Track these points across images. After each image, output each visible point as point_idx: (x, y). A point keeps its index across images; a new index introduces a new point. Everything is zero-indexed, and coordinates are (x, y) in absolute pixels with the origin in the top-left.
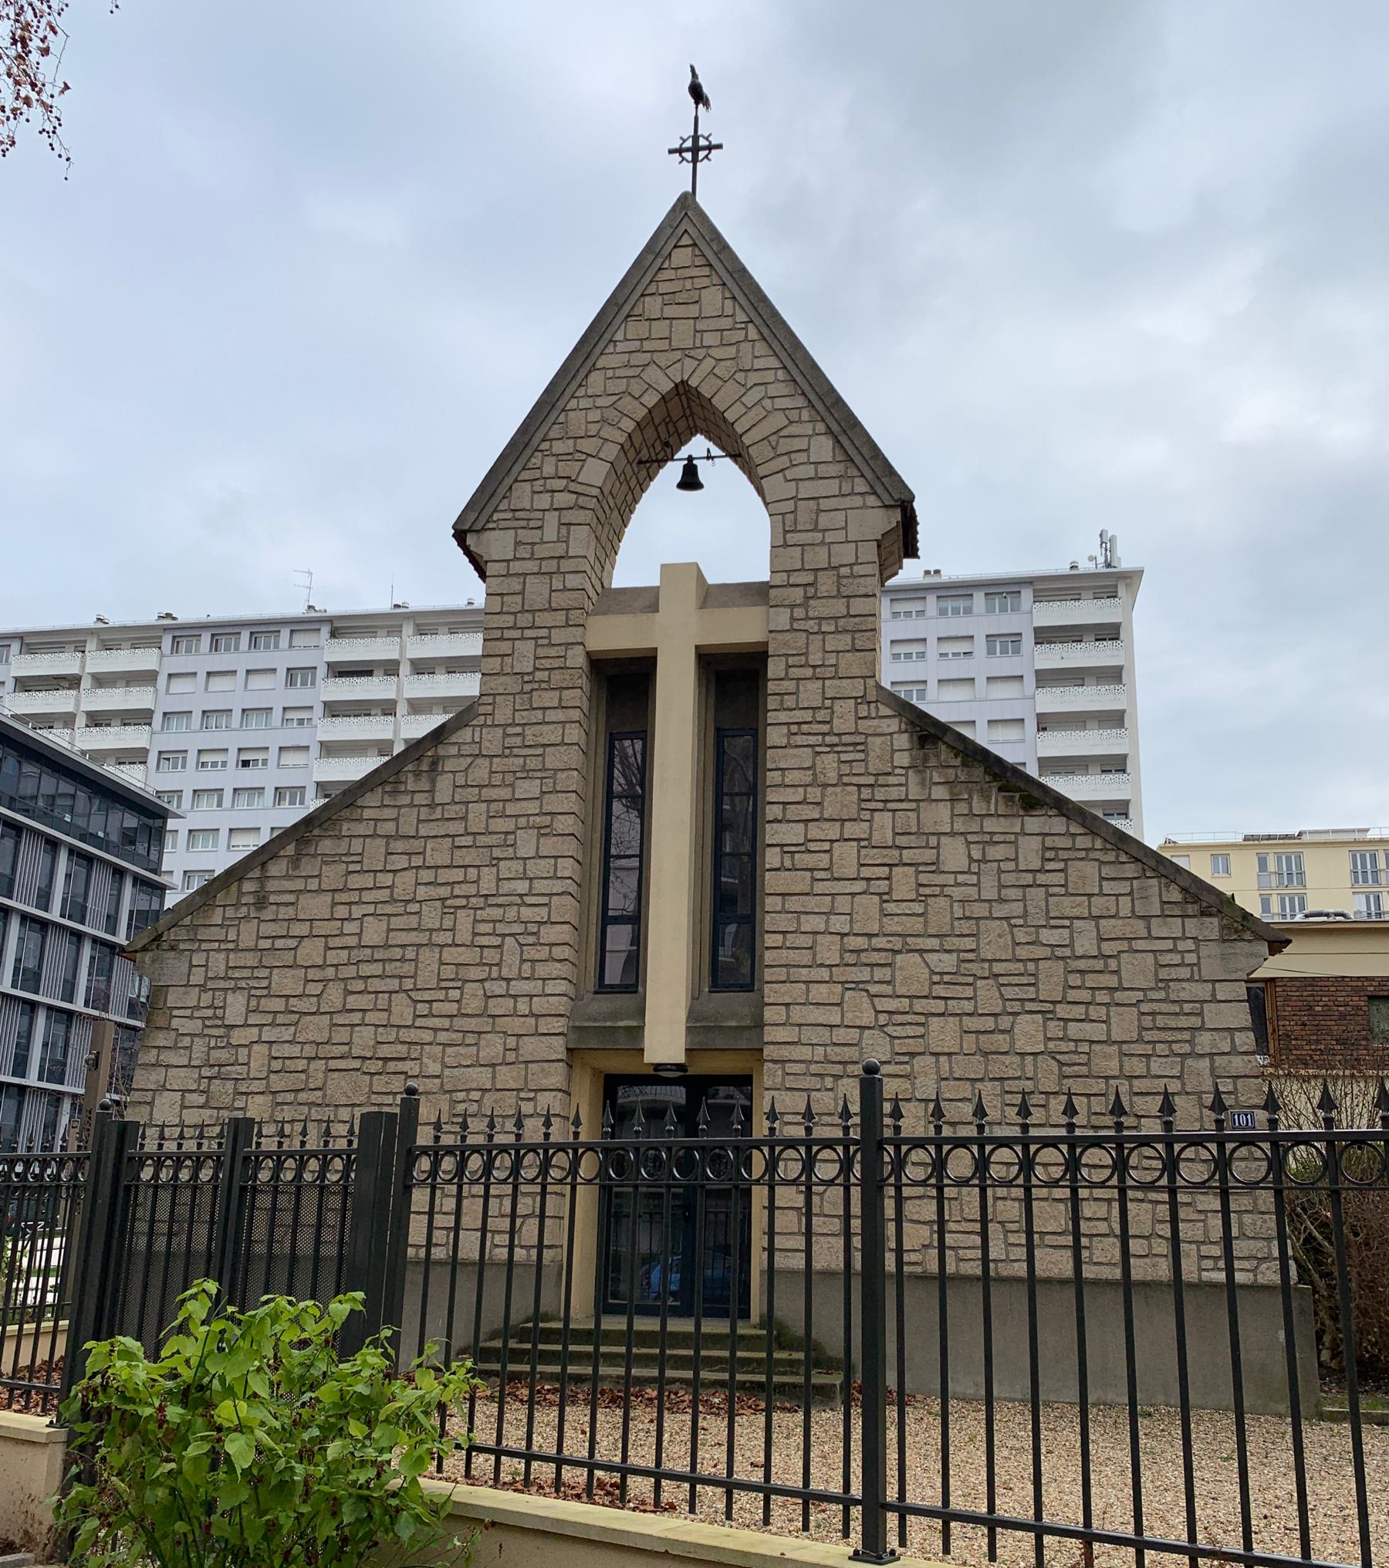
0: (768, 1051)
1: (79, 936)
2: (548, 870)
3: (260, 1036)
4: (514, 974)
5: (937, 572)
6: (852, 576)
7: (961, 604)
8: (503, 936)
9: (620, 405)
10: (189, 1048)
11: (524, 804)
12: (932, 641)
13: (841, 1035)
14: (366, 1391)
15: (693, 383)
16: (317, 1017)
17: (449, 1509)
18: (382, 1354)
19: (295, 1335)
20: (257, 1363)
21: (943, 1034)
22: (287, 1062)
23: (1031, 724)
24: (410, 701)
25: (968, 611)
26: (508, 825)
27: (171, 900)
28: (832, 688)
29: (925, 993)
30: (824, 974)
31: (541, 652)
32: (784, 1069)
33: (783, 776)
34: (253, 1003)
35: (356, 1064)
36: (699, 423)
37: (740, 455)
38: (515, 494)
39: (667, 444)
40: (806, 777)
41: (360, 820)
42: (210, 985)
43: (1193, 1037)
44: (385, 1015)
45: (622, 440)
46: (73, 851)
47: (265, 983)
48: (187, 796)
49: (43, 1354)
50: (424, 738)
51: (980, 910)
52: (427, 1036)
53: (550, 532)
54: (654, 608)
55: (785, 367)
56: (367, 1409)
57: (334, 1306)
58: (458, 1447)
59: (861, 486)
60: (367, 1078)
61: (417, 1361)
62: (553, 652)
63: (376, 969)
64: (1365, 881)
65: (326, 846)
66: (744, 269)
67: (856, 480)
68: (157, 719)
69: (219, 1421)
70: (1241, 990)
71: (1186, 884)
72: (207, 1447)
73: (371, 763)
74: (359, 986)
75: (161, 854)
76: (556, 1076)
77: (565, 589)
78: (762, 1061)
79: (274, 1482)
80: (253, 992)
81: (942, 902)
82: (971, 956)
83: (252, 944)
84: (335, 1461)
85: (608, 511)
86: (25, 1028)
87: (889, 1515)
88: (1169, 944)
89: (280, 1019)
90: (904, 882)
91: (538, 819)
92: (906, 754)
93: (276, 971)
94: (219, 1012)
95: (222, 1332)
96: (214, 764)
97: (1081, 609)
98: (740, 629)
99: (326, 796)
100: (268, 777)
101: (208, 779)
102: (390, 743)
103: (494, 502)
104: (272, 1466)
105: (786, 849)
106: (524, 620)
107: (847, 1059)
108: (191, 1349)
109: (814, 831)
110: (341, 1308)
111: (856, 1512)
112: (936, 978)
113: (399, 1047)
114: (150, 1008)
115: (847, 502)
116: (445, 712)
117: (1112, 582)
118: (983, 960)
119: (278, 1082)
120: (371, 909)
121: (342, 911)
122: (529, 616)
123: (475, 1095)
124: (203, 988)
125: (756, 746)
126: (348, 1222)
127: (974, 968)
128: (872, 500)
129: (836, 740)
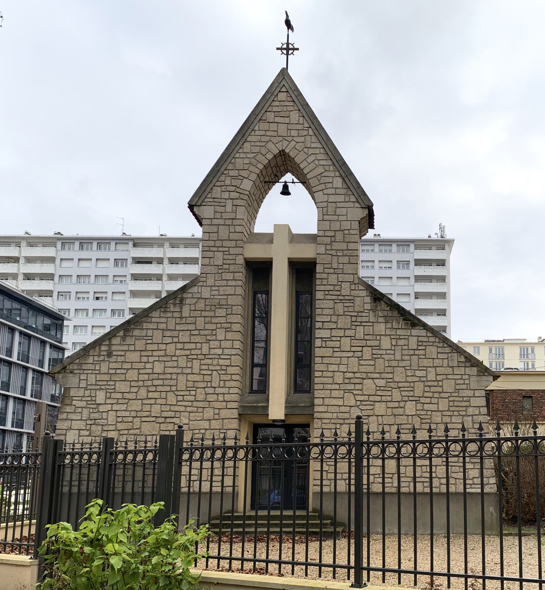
0: (316, 415)
1: (26, 369)
2: (230, 346)
3: (112, 408)
4: (217, 385)
5: (379, 235)
6: (349, 234)
7: (388, 248)
8: (212, 370)
9: (257, 158)
10: (81, 413)
11: (219, 318)
12: (377, 262)
13: (343, 409)
14: (167, 538)
15: (287, 151)
16: (136, 401)
17: (200, 580)
18: (172, 524)
19: (137, 519)
20: (121, 530)
21: (380, 408)
22: (124, 418)
23: (413, 296)
24: (168, 275)
25: (390, 251)
26: (213, 327)
27: (67, 354)
28: (341, 277)
29: (374, 394)
30: (337, 387)
31: (226, 257)
32: (321, 421)
33: (322, 311)
34: (108, 395)
35: (154, 419)
36: (289, 168)
37: (305, 183)
38: (214, 191)
39: (276, 176)
40: (331, 312)
41: (151, 322)
42: (89, 387)
43: (467, 409)
44: (165, 400)
45: (258, 172)
46: (21, 333)
47: (113, 387)
48: (72, 312)
49: (26, 533)
50: (178, 290)
51: (394, 364)
52: (182, 409)
53: (229, 208)
54: (271, 242)
55: (323, 148)
56: (167, 544)
57: (152, 507)
58: (203, 557)
59: (353, 199)
60: (158, 424)
61: (186, 526)
62: (230, 257)
63: (160, 382)
64: (524, 357)
65: (137, 333)
66: (308, 104)
67: (351, 196)
68: (56, 278)
69: (106, 552)
70: (483, 393)
71: (467, 355)
72: (102, 562)
73: (152, 301)
74: (153, 389)
75: (62, 335)
76: (235, 424)
77: (235, 232)
78: (314, 419)
79: (131, 573)
80: (108, 391)
81: (381, 361)
82: (391, 380)
83: (106, 371)
84: (155, 564)
85: (252, 201)
86: (4, 406)
87: (364, 571)
88: (460, 377)
89: (120, 401)
90: (367, 353)
91: (225, 325)
92: (369, 305)
93: (117, 382)
94: (93, 399)
95: (106, 519)
96: (83, 298)
97: (431, 253)
98: (306, 252)
99: (133, 314)
100: (108, 304)
101: (81, 305)
102: (160, 292)
103: (205, 194)
104: (130, 567)
105: (323, 339)
106: (218, 244)
107: (345, 418)
108: (93, 526)
109: (334, 333)
110: (155, 508)
111: (352, 571)
112: (378, 388)
113: (171, 413)
114: (63, 398)
115: (347, 205)
116: (183, 280)
117: (443, 244)
118: (395, 382)
119: (120, 426)
120: (157, 358)
121: (145, 359)
122: (220, 242)
123: (203, 431)
124: (86, 389)
125: (312, 298)
126: (156, 479)
127: (392, 385)
128: (357, 205)
129: (342, 298)
